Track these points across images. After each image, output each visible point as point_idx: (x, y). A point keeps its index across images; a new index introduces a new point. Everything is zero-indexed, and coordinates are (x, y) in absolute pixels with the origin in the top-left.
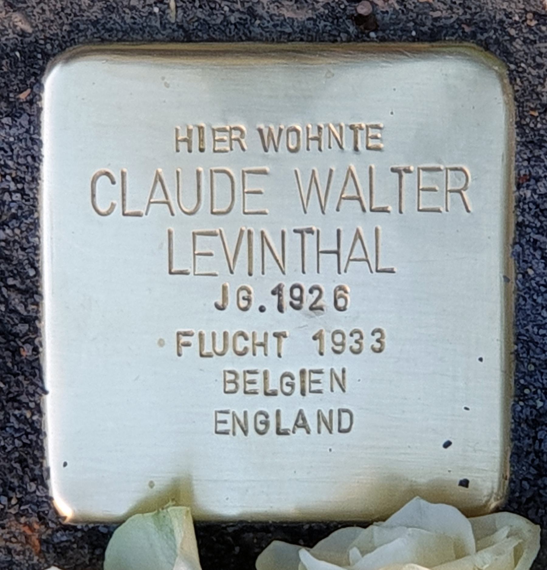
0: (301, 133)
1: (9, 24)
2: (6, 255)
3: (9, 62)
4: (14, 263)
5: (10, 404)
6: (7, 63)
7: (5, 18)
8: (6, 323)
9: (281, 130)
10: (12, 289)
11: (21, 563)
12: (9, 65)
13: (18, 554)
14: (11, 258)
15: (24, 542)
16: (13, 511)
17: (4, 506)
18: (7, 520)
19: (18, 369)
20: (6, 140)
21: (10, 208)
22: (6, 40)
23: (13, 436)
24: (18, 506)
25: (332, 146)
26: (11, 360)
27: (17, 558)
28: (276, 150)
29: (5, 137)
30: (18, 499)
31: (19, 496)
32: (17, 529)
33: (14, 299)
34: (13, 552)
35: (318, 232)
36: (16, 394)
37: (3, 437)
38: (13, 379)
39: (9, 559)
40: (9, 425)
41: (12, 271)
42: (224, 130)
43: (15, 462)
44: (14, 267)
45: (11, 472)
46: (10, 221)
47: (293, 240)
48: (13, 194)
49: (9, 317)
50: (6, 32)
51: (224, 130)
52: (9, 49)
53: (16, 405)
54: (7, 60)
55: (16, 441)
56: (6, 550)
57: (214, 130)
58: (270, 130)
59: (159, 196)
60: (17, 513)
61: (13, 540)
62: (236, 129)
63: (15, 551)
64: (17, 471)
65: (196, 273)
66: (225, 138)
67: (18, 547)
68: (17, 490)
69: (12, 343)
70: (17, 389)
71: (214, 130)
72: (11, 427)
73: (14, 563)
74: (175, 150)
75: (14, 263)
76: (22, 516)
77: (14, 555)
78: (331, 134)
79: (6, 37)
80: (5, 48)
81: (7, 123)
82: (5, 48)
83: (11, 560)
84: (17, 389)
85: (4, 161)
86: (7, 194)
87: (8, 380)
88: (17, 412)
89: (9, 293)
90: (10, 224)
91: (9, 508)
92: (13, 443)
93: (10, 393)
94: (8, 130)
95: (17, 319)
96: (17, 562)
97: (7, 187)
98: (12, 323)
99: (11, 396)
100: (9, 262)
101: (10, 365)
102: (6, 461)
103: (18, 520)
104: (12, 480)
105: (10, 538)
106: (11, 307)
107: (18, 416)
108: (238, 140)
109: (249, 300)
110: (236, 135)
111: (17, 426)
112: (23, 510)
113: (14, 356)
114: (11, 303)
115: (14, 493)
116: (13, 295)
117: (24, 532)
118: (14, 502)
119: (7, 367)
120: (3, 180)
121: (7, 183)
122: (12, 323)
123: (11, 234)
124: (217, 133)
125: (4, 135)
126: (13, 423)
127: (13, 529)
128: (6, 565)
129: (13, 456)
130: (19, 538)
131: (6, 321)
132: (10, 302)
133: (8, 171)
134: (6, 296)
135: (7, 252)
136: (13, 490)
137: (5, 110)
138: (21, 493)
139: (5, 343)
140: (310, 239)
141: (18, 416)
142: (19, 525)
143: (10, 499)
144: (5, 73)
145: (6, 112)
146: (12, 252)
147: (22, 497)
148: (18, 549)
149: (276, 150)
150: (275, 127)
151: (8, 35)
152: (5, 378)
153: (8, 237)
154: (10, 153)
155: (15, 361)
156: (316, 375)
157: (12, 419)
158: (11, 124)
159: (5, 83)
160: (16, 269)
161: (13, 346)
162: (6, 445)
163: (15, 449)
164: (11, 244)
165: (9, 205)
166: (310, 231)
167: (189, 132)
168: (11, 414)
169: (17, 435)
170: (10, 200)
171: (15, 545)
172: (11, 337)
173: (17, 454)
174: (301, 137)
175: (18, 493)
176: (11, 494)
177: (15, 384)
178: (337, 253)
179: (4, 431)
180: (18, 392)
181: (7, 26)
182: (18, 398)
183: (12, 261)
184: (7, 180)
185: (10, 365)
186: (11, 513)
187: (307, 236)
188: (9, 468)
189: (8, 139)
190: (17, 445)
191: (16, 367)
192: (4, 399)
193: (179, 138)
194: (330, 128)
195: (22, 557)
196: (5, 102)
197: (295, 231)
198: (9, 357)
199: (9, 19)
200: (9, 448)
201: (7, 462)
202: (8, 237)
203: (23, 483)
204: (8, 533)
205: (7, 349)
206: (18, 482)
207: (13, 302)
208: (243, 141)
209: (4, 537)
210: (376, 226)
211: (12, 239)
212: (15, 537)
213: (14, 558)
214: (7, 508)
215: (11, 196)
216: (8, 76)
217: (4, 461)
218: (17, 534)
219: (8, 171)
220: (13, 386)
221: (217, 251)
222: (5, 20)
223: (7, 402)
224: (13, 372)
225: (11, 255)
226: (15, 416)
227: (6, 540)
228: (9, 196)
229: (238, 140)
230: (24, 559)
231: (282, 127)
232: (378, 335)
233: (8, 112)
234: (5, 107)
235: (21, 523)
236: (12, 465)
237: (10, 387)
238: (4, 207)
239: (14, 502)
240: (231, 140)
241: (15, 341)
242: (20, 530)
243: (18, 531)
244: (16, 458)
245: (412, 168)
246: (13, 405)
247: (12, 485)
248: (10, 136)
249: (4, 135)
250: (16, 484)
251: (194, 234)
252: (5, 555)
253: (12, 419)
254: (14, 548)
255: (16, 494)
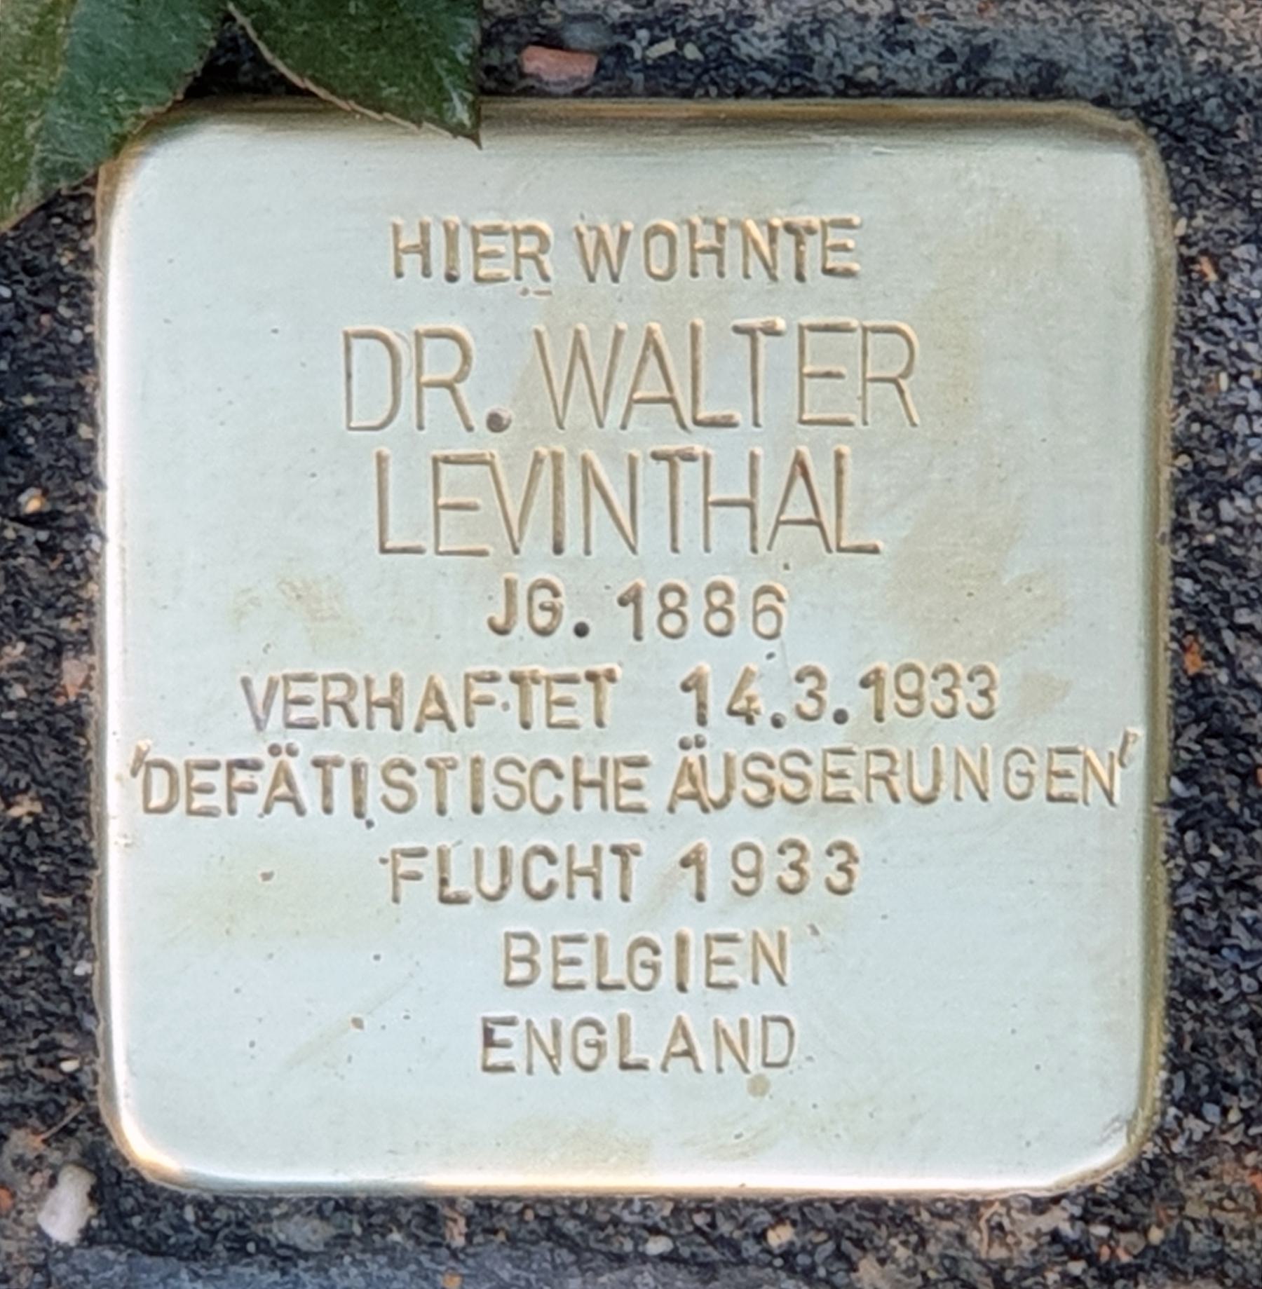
0: (679, 240)
1: (1253, 35)
2: (1234, 556)
3: (1251, 119)
4: (1251, 574)
5: (1232, 895)
6: (1247, 121)
7: (1244, 21)
8: (1229, 712)
9: (624, 235)
10: (1243, 634)
11: (1244, 1258)
12: (1250, 126)
13: (1238, 1237)
14: (1244, 561)
15: (1253, 1209)
16: (1231, 1138)
17: (1212, 1124)
18: (1215, 1159)
19: (1252, 817)
20: (1242, 296)
21: (1246, 453)
22: (1246, 69)
23: (1236, 967)
24: (1242, 1126)
25: (751, 272)
26: (1236, 795)
27: (1236, 1244)
28: (615, 278)
29: (1241, 290)
30: (1242, 1110)
31: (1246, 1104)
32: (1235, 1181)
33: (1248, 658)
34: (1226, 1231)
35: (707, 458)
36: (1246, 871)
37: (1215, 970)
38: (1241, 837)
39: (1216, 1248)
40: (1228, 941)
41: (1245, 594)
42: (497, 231)
43: (1242, 1028)
44: (1252, 584)
45: (1230, 1048)
46: (1248, 479)
47: (654, 476)
48: (1254, 417)
49: (1236, 696)
50: (1246, 53)
51: (497, 231)
52: (1251, 90)
53: (1245, 896)
54: (1247, 115)
55: (1246, 980)
56: (1212, 1228)
57: (475, 232)
58: (600, 233)
59: (652, 386)
60: (1241, 1143)
61: (1228, 1204)
62: (531, 230)
63: (1232, 1229)
64: (1243, 1049)
65: (441, 549)
66: (502, 249)
67: (1240, 1222)
68: (1242, 1089)
69: (1241, 757)
70: (1250, 861)
71: (475, 232)
72: (1232, 947)
73: (1229, 1257)
74: (392, 273)
75: (1251, 574)
76: (1250, 1149)
77: (1228, 1240)
78: (751, 246)
79: (1245, 63)
80: (1242, 88)
81: (1247, 257)
82: (1242, 88)
83: (1221, 1251)
84: (1250, 861)
85: (1239, 344)
86: (1241, 418)
87: (1230, 839)
88: (1247, 913)
89: (1239, 642)
90: (1246, 486)
91: (1223, 1132)
92: (1238, 983)
93: (1234, 868)
94: (1246, 274)
95: (1254, 701)
96: (1234, 1255)
97: (1242, 403)
98: (1242, 711)
99: (1235, 876)
100: (1240, 571)
101: (1234, 806)
102: (1221, 1023)
103: (1239, 1159)
104: (1231, 1069)
105: (1221, 1200)
106: (1241, 675)
107: (1250, 922)
108: (533, 257)
109: (554, 610)
110: (529, 245)
111: (1246, 946)
112: (1254, 1138)
113: (1244, 786)
114: (1241, 666)
115: (1235, 1098)
116: (1247, 648)
117: (1254, 1186)
118: (1234, 1116)
119: (1229, 810)
120: (1234, 385)
121: (1243, 394)
122: (1242, 711)
123: (1249, 510)
124: (483, 238)
125: (1239, 285)
126: (1237, 937)
127: (1227, 1180)
128: (1209, 1260)
129: (1236, 1014)
130: (1241, 1200)
131: (1228, 708)
132: (1237, 662)
133: (1244, 366)
134: (1232, 650)
135: (1236, 551)
136: (1234, 1091)
137: (1242, 227)
138: (1251, 1097)
139: (1225, 757)
140: (689, 473)
141: (1250, 922)
142: (1240, 1171)
143: (1225, 1111)
144: (1243, 144)
145: (1243, 233)
146: (1249, 550)
147: (1252, 1108)
148: (1238, 1226)
149: (615, 278)
150: (612, 226)
151: (1249, 58)
152: (1224, 835)
153: (1241, 517)
154: (1251, 326)
155: (1247, 796)
156: (632, 770)
157: (1237, 929)
158: (1253, 259)
159: (1242, 166)
160: (1254, 588)
161: (1242, 764)
162: (1222, 989)
163: (1243, 996)
164: (1247, 532)
165: (1244, 443)
166: (689, 457)
167: (424, 229)
168: (1233, 917)
169: (1248, 965)
170: (1248, 432)
171: (1231, 1215)
172: (1240, 744)
173: (1244, 1009)
174: (679, 249)
175: (1244, 1098)
176: (1228, 1099)
177: (1245, 851)
178: (750, 505)
179: (1216, 956)
180: (1250, 867)
181: (1247, 37)
182: (1249, 882)
183: (1245, 570)
184: (1242, 388)
185: (1234, 806)
186: (1226, 1143)
187: (684, 468)
188: (1225, 1041)
189: (1248, 293)
190: (1245, 988)
191: (1247, 812)
192: (1220, 884)
193: (402, 245)
194: (746, 234)
195: (1246, 1242)
196: (1242, 209)
197: (656, 456)
198: (1235, 788)
199: (1253, 22)
200: (1228, 995)
201: (1222, 1028)
202: (1241, 517)
203: (1254, 1075)
204: (1217, 1189)
205: (1230, 771)
206: (1244, 1072)
207: (1246, 664)
208: (544, 258)
209: (1206, 1197)
210: (751, 448)
211: (1248, 521)
212: (1231, 1197)
213: (1229, 1245)
214: (1216, 1131)
215: (1250, 422)
216: (1251, 152)
217: (1216, 1024)
218: (1235, 1193)
219: (1244, 366)
220: (1241, 853)
221: (486, 501)
222: (1245, 26)
223: (1227, 889)
224: (1241, 821)
225: (1244, 557)
226: (1243, 921)
227: (1211, 1205)
228: (1246, 424)
229: (533, 257)
230: (1251, 1248)
231: (628, 225)
232: (811, 683)
233: (1249, 232)
234: (1243, 222)
235: (1245, 1167)
236: (1232, 1035)
237: (1234, 857)
238: (1233, 446)
239: (1234, 1116)
240: (518, 256)
241: (1247, 753)
242: (1243, 1181)
243: (1238, 1184)
244: (1241, 1019)
245: (781, 324)
246: (1238, 898)
247: (1229, 1080)
248: (1250, 285)
249: (1239, 285)
250: (1240, 1076)
251: (435, 461)
252: (1208, 1237)
253: (1237, 929)
254: (1227, 1222)
255: (1240, 1100)
